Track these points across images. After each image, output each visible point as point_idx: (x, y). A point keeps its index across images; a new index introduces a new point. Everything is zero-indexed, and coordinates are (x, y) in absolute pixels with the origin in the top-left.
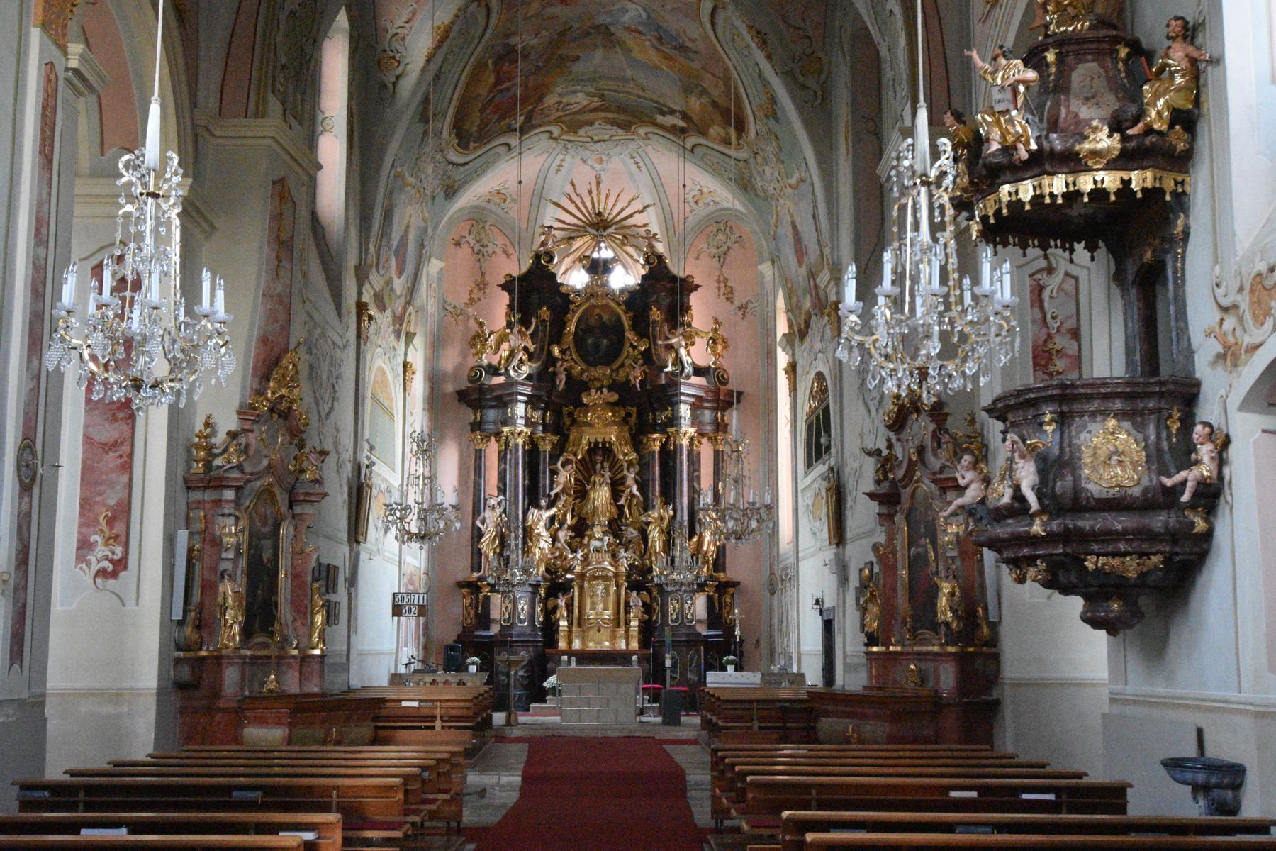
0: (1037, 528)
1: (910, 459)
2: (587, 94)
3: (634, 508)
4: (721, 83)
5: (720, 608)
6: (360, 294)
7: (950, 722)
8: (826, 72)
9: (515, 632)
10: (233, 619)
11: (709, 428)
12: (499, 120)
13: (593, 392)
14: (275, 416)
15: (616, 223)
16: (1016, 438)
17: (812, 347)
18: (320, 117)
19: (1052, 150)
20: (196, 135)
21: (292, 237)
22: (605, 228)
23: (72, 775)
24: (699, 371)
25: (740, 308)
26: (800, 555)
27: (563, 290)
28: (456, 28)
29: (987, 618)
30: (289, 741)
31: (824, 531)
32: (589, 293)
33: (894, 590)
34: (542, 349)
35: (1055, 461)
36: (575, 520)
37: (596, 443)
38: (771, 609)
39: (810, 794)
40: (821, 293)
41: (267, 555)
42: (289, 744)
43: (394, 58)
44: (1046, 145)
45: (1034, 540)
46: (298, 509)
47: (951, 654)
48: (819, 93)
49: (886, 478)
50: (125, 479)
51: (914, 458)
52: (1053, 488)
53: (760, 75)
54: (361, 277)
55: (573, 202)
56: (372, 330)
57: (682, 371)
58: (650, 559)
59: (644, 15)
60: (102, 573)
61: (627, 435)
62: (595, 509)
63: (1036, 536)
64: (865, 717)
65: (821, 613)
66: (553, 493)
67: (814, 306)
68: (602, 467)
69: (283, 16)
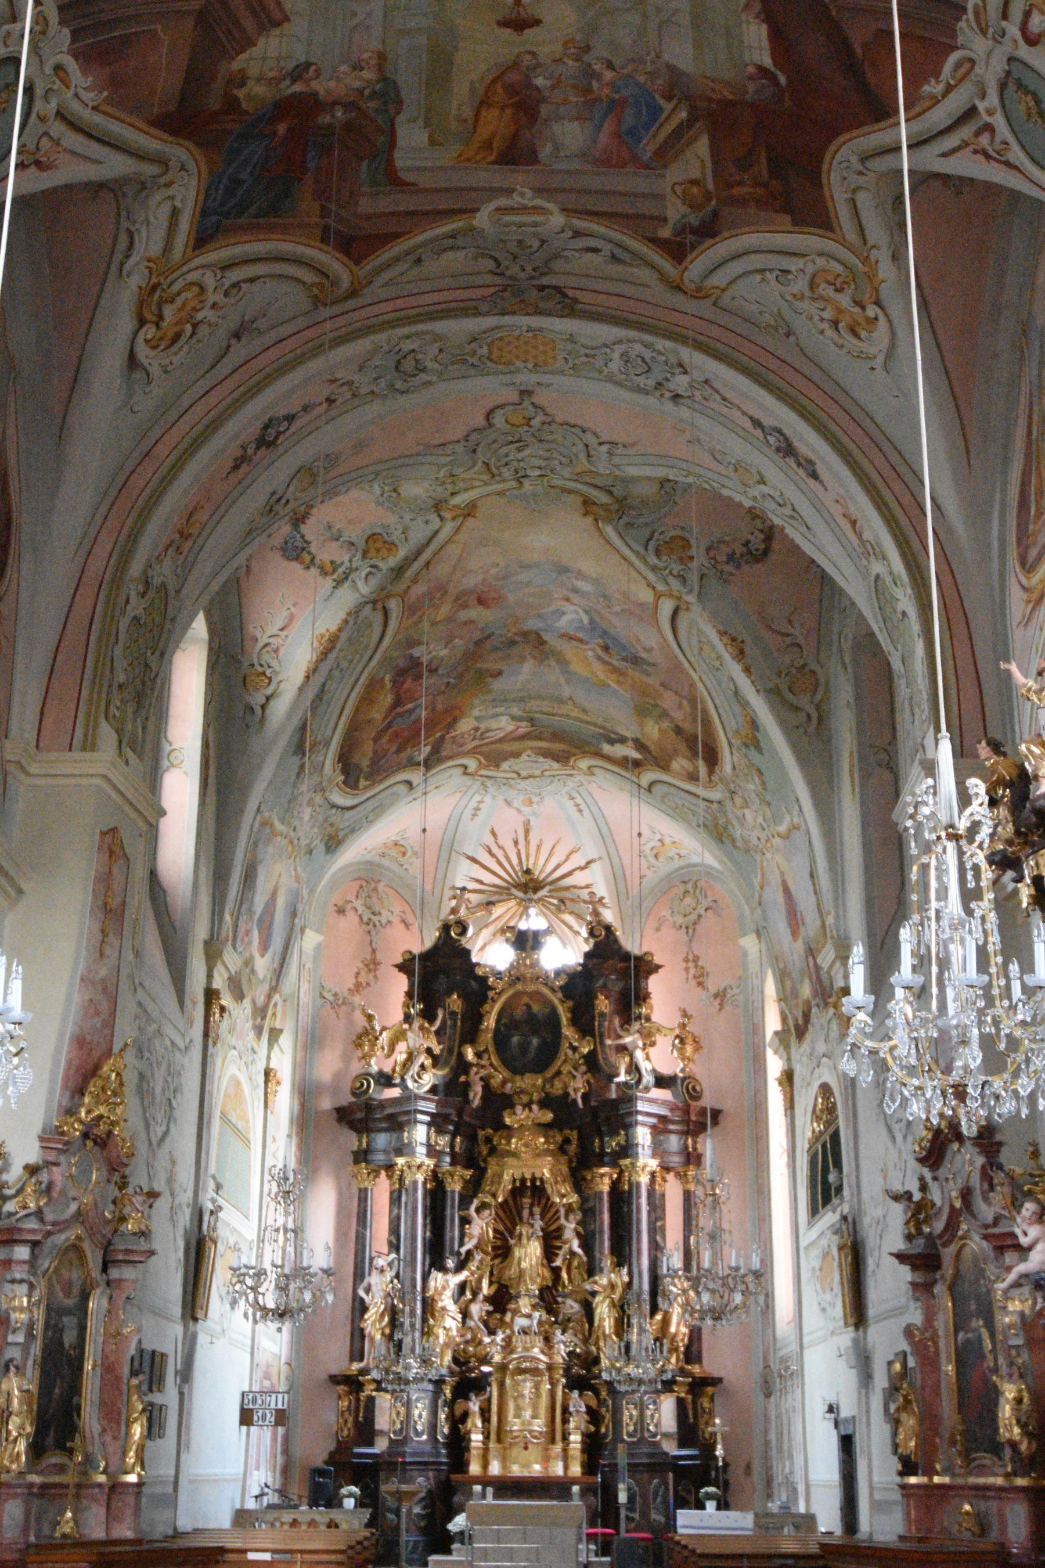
1: (952, 1206)
2: (514, 718)
5: (695, 1417)
6: (210, 976)
12: (398, 751)
13: (519, 1109)
14: (89, 1144)
18: (167, 748)
24: (662, 1081)
25: (716, 996)
27: (480, 972)
28: (344, 636)
31: (837, 1307)
32: (515, 976)
34: (450, 1051)
36: (494, 1287)
37: (523, 1180)
40: (824, 976)
41: (69, 1338)
43: (264, 674)
46: (114, 1273)
49: (920, 1232)
51: (958, 1204)
53: (736, 693)
55: (492, 855)
59: (586, 620)
61: (565, 1169)
62: (521, 1273)
65: (836, 1424)
66: (463, 1250)
67: (815, 995)
68: (531, 1214)
69: (124, 624)
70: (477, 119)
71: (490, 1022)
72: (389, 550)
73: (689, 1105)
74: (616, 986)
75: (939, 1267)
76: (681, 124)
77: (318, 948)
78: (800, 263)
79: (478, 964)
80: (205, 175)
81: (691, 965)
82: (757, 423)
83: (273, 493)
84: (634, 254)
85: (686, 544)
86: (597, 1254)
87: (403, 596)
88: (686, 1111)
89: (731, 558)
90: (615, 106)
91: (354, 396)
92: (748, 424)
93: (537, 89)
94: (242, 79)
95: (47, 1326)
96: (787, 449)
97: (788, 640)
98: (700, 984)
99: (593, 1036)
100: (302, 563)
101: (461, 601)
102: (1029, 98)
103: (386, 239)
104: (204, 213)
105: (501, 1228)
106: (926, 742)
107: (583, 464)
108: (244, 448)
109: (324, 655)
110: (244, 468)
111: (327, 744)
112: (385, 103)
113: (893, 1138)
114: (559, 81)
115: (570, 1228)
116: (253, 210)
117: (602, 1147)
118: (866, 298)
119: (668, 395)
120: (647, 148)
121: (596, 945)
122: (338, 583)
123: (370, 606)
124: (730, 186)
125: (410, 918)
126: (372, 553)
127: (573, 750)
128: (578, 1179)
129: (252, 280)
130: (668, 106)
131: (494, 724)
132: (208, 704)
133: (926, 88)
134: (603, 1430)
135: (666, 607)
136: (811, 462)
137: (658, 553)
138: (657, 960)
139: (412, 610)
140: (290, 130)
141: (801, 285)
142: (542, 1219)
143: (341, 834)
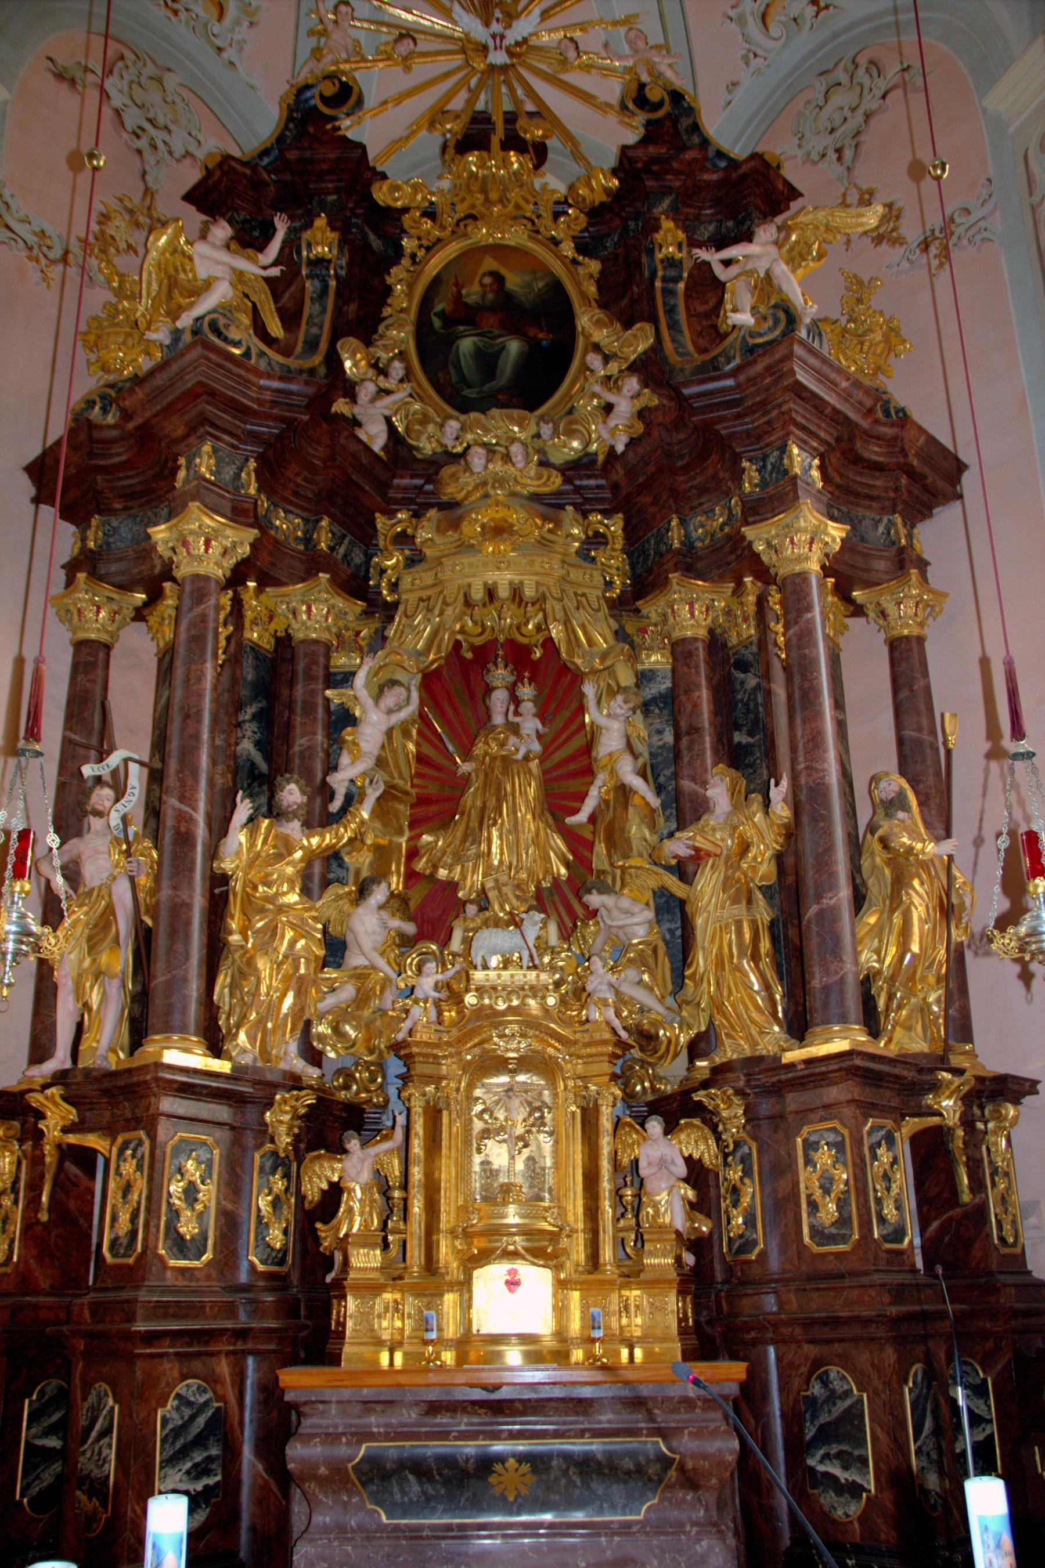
5: (977, 1185)
27: (381, 194)
39: (165, 1280)
99: (654, 320)
142: (541, 716)
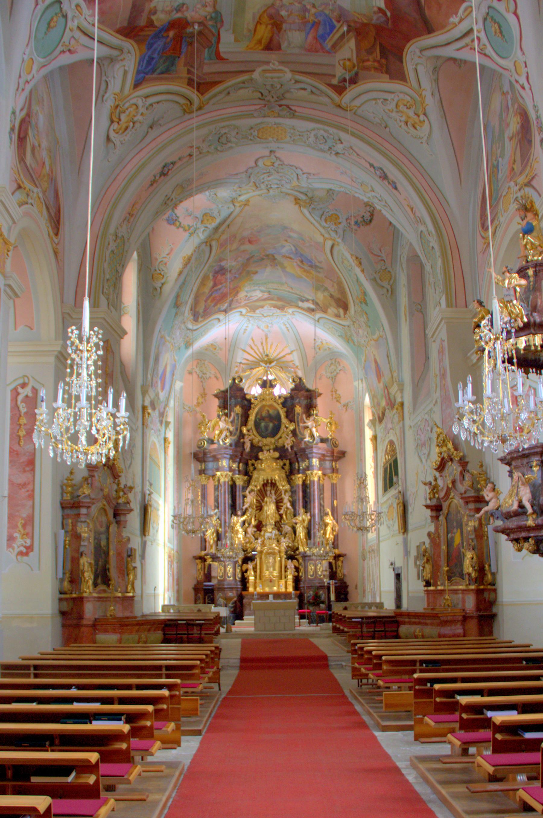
0: (530, 522)
1: (448, 487)
2: (262, 291)
3: (288, 515)
4: (335, 285)
6: (143, 401)
7: (473, 625)
8: (393, 279)
9: (225, 583)
10: (88, 576)
11: (328, 471)
12: (215, 305)
13: (265, 452)
14: (106, 468)
15: (277, 360)
16: (520, 474)
17: (386, 426)
18: (123, 306)
19: (535, 322)
20: (63, 318)
21: (113, 371)
22: (270, 363)
23: (42, 654)
24: (323, 440)
25: (344, 406)
26: (381, 539)
27: (248, 397)
28: (193, 258)
29: (490, 570)
30: (120, 641)
31: (396, 525)
32: (262, 398)
33: (439, 556)
34: (237, 430)
35: (539, 487)
36: (257, 522)
37: (267, 481)
38: (363, 567)
40: (392, 397)
41: (103, 543)
42: (120, 643)
43: (160, 274)
44: (532, 320)
45: (529, 529)
46: (118, 518)
47: (472, 590)
48: (390, 290)
49: (434, 497)
50: (30, 503)
51: (450, 486)
52: (539, 501)
53: (358, 280)
54: (144, 393)
55: (252, 348)
56: (149, 420)
57: (314, 440)
58: (298, 542)
59: (294, 249)
60: (21, 553)
61: (284, 475)
62: (267, 516)
63: (529, 527)
64: (426, 624)
65: (394, 569)
66: (244, 508)
67: (387, 404)
68: (271, 493)
69: (108, 253)
70: (255, 30)
71: (252, 418)
72: (212, 220)
73: (333, 450)
74: (304, 402)
75: (441, 510)
76: (344, 33)
77: (181, 388)
78: (392, 96)
79: (247, 394)
80: (138, 54)
81: (334, 393)
82: (372, 165)
83: (166, 196)
84: (322, 92)
85: (337, 217)
86: (297, 508)
87: (218, 240)
88: (333, 452)
89: (356, 223)
90: (315, 25)
91: (200, 153)
92: (368, 166)
93: (282, 16)
94: (154, 12)
95: (95, 538)
96: (384, 177)
97: (380, 258)
98: (337, 401)
99: (294, 422)
100: (176, 226)
101: (242, 241)
102: (496, 25)
103: (215, 83)
104: (138, 72)
105: (259, 499)
106: (441, 301)
107: (295, 183)
108: (155, 176)
109: (185, 266)
110: (155, 185)
111: (187, 303)
112: (216, 23)
113: (421, 461)
114: (291, 13)
115: (286, 498)
116: (158, 71)
117: (299, 467)
118: (420, 112)
119: (333, 153)
120: (329, 44)
121: (296, 386)
122: (191, 234)
123: (204, 244)
124: (364, 61)
125: (218, 376)
126: (205, 221)
127: (286, 304)
128: (289, 480)
129: (158, 103)
130: (338, 25)
131: (254, 294)
132: (138, 287)
133: (451, 20)
134: (300, 574)
135: (329, 244)
136: (395, 183)
137: (326, 221)
138: (320, 391)
139: (222, 245)
140: (175, 34)
141: (392, 106)
143: (191, 341)
